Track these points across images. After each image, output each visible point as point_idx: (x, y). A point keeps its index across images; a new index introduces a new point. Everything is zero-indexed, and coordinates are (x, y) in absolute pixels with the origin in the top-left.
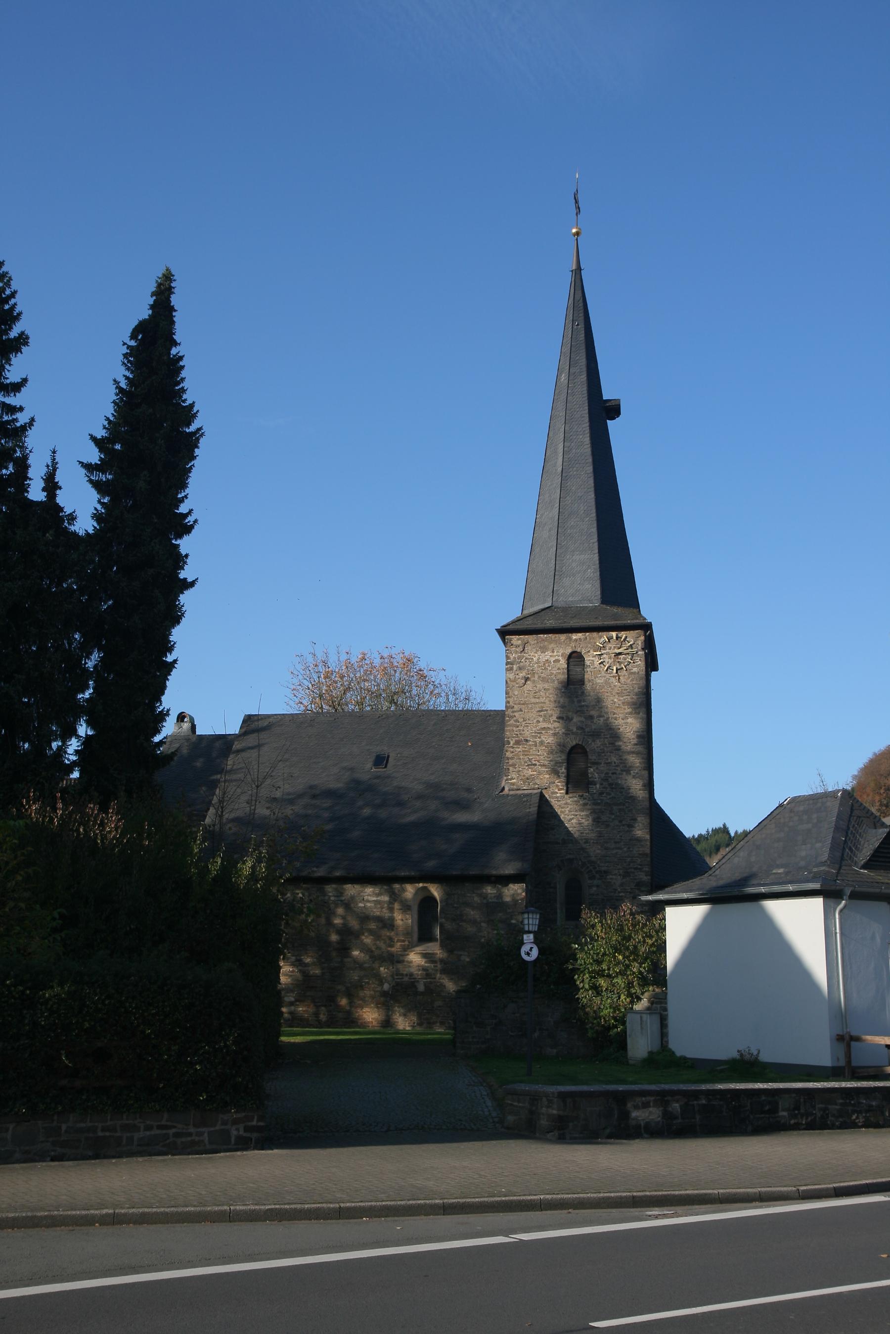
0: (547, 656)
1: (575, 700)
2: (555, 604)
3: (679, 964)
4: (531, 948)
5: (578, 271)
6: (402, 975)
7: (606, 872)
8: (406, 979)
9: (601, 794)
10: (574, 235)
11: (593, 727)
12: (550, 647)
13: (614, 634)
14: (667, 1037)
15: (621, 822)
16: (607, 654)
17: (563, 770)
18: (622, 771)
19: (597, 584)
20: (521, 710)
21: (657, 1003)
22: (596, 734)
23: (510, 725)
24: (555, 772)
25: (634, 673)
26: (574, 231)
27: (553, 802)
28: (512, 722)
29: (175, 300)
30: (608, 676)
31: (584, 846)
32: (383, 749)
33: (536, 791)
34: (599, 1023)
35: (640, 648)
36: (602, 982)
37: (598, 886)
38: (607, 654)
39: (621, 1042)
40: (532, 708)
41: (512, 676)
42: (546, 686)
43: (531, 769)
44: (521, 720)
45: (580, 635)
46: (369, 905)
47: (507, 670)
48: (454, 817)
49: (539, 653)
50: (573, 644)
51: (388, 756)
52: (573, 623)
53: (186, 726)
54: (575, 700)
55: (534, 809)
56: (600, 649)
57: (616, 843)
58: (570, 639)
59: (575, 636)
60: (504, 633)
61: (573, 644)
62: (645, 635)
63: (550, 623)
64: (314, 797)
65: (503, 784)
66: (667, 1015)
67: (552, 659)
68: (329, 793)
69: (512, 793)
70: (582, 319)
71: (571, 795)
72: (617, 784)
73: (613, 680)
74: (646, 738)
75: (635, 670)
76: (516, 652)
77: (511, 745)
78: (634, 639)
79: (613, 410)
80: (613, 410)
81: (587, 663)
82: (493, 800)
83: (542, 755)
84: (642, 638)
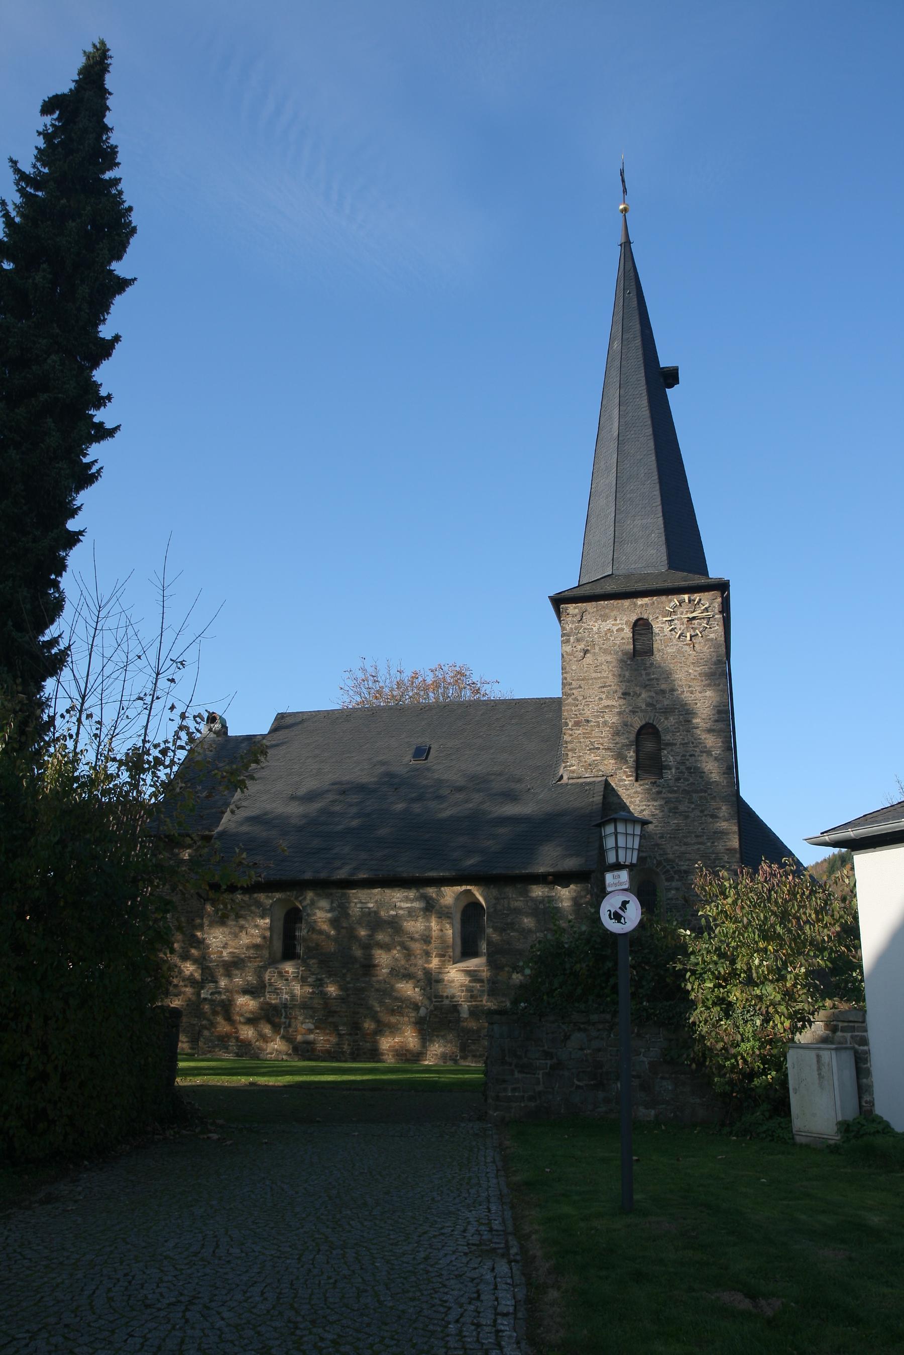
0: (608, 624)
1: (643, 672)
2: (615, 572)
3: (884, 958)
4: (625, 903)
5: (627, 245)
6: (442, 997)
7: (686, 872)
8: (446, 1002)
9: (678, 779)
10: (622, 211)
11: (666, 703)
12: (612, 614)
13: (686, 597)
14: (871, 1094)
15: (702, 811)
16: (680, 619)
17: (632, 753)
18: (701, 752)
19: (663, 549)
20: (580, 687)
21: (843, 1030)
22: (667, 711)
23: (568, 705)
24: (620, 757)
25: (712, 640)
26: (622, 207)
27: (621, 791)
28: (570, 700)
29: (109, 81)
30: (680, 644)
31: (659, 841)
32: (424, 740)
33: (600, 779)
34: (734, 1067)
35: (716, 611)
36: (736, 995)
37: (677, 889)
38: (680, 619)
39: (779, 1103)
40: (592, 684)
41: (568, 648)
42: (609, 658)
43: (592, 756)
44: (580, 698)
45: (646, 599)
46: (401, 912)
47: (563, 642)
48: (504, 809)
49: (600, 622)
50: (638, 610)
51: (430, 748)
52: (640, 587)
53: (217, 726)
54: (643, 672)
55: (598, 799)
56: (671, 614)
57: (697, 836)
58: (635, 605)
59: (640, 602)
60: (559, 601)
61: (638, 610)
62: (722, 596)
63: (610, 587)
64: (344, 792)
65: (561, 771)
66: (868, 1052)
67: (615, 628)
68: (361, 788)
69: (571, 781)
70: (634, 287)
71: (642, 782)
72: (697, 768)
73: (687, 648)
74: (725, 717)
75: (712, 636)
76: (573, 622)
77: (570, 726)
78: (709, 601)
79: (671, 377)
80: (671, 377)
81: (656, 630)
82: (550, 790)
83: (603, 736)
84: (719, 600)
